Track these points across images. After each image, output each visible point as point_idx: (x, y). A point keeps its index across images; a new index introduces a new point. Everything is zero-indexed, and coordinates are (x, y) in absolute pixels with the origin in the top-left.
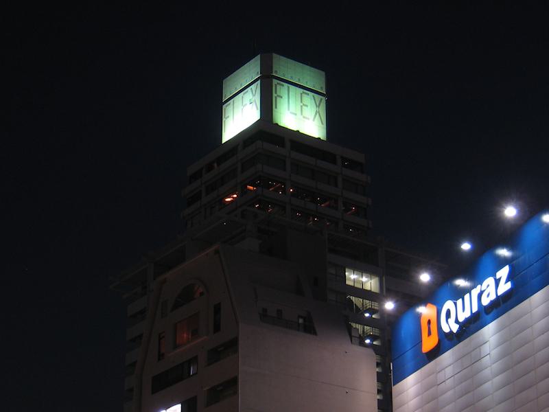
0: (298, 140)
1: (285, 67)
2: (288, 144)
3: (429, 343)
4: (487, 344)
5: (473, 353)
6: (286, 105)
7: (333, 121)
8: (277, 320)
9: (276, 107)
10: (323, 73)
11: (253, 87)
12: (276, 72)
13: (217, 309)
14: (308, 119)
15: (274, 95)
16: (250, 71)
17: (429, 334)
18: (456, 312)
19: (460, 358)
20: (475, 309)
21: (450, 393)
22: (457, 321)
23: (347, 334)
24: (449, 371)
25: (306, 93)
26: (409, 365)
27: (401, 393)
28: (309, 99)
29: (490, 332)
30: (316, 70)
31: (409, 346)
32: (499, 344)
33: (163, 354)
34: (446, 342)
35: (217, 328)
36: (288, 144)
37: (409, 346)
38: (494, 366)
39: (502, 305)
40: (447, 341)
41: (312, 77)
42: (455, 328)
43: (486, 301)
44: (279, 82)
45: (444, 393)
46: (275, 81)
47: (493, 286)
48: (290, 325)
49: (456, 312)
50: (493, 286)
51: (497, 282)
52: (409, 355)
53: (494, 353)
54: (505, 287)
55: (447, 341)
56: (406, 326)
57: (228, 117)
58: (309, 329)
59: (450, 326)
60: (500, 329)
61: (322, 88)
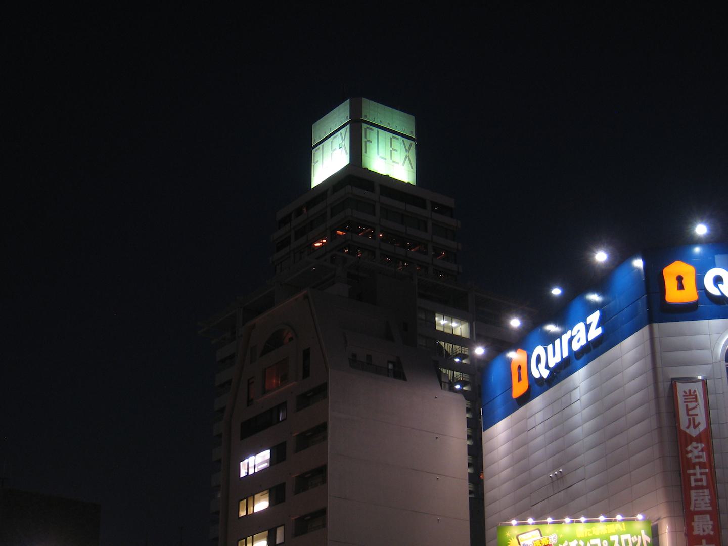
0: (387, 185)
1: (375, 112)
2: (377, 189)
3: (519, 389)
4: (577, 391)
6: (375, 141)
8: (355, 362)
9: (366, 152)
10: (413, 118)
11: (342, 131)
12: (366, 116)
13: (307, 354)
15: (364, 139)
16: (340, 115)
17: (520, 379)
19: (551, 404)
21: (539, 428)
22: (547, 367)
24: (539, 417)
25: (393, 137)
26: (500, 410)
28: (398, 143)
29: (580, 377)
31: (499, 392)
35: (306, 373)
36: (377, 189)
37: (499, 392)
38: (585, 411)
39: (592, 350)
40: (537, 386)
41: (402, 122)
42: (545, 373)
43: (576, 347)
44: (368, 126)
46: (364, 126)
48: (379, 370)
51: (588, 327)
53: (585, 398)
54: (595, 332)
55: (537, 386)
56: (496, 373)
58: (399, 374)
60: (591, 374)
61: (411, 133)
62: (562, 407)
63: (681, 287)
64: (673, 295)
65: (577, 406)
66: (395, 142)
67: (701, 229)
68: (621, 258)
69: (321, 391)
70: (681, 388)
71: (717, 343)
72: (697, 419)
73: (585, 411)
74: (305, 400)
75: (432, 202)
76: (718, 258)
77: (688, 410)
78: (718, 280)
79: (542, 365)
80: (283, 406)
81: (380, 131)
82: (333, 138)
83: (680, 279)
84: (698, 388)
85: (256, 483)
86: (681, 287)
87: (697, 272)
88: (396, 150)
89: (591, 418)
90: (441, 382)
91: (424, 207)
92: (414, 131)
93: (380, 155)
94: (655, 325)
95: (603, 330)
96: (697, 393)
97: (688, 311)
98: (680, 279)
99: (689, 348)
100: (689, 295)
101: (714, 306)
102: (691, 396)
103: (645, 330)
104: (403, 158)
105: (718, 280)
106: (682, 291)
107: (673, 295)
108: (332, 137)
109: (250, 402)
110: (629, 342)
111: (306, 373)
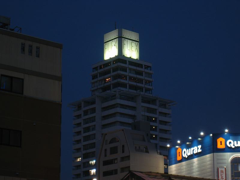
0: (131, 61)
1: (127, 33)
2: (128, 62)
3: (179, 158)
4: (195, 164)
5: (191, 165)
6: (126, 44)
7: (142, 52)
8: (138, 150)
9: (123, 48)
10: (138, 34)
11: (115, 40)
12: (123, 36)
13: (123, 146)
14: (133, 51)
15: (123, 44)
16: (114, 34)
17: (179, 156)
18: (187, 153)
19: (187, 165)
20: (192, 154)
21: (184, 170)
22: (187, 155)
23: (156, 152)
24: (184, 167)
25: (133, 42)
26: (173, 162)
27: (171, 169)
28: (134, 44)
29: (195, 160)
30: (135, 33)
31: (173, 157)
32: (198, 164)
33: (106, 155)
34: (183, 159)
35: (123, 152)
36: (128, 62)
37: (173, 157)
38: (196, 169)
39: (198, 155)
40: (184, 159)
41: (135, 36)
42: (186, 157)
43: (195, 153)
44: (124, 39)
45: (183, 172)
46: (123, 39)
47: (197, 149)
48: (142, 151)
49: (187, 153)
50: (197, 149)
51: (198, 148)
52: (173, 159)
53: (196, 166)
54: (200, 151)
55: (184, 159)
56: (173, 151)
57: (106, 48)
58: (147, 152)
59: (185, 156)
60: (198, 160)
61: (138, 39)
62: (190, 166)
63: (221, 144)
64: (219, 146)
65: (194, 167)
66: (133, 43)
67: (227, 131)
68: (207, 134)
69: (128, 157)
70: (220, 170)
71: (229, 159)
72: (223, 177)
73: (197, 173)
74: (123, 159)
75: (145, 65)
76: (231, 137)
77: (221, 175)
78: (230, 143)
79: (186, 154)
80: (117, 159)
81: (128, 40)
82: (112, 42)
83: (221, 142)
84: (224, 170)
85: (92, 167)
86: (221, 144)
87: (225, 140)
88: (133, 46)
89: (198, 171)
90: (157, 152)
91: (142, 68)
92: (138, 38)
93: (128, 49)
94: (215, 153)
95: (202, 150)
96: (224, 171)
97: (223, 150)
98: (221, 142)
99: (222, 159)
100: (223, 146)
101: (229, 149)
102: (222, 172)
103: (212, 154)
104: (135, 49)
105: (230, 143)
106: (221, 145)
107: (219, 146)
108: (111, 41)
109: (106, 156)
110: (208, 156)
111: (123, 152)
